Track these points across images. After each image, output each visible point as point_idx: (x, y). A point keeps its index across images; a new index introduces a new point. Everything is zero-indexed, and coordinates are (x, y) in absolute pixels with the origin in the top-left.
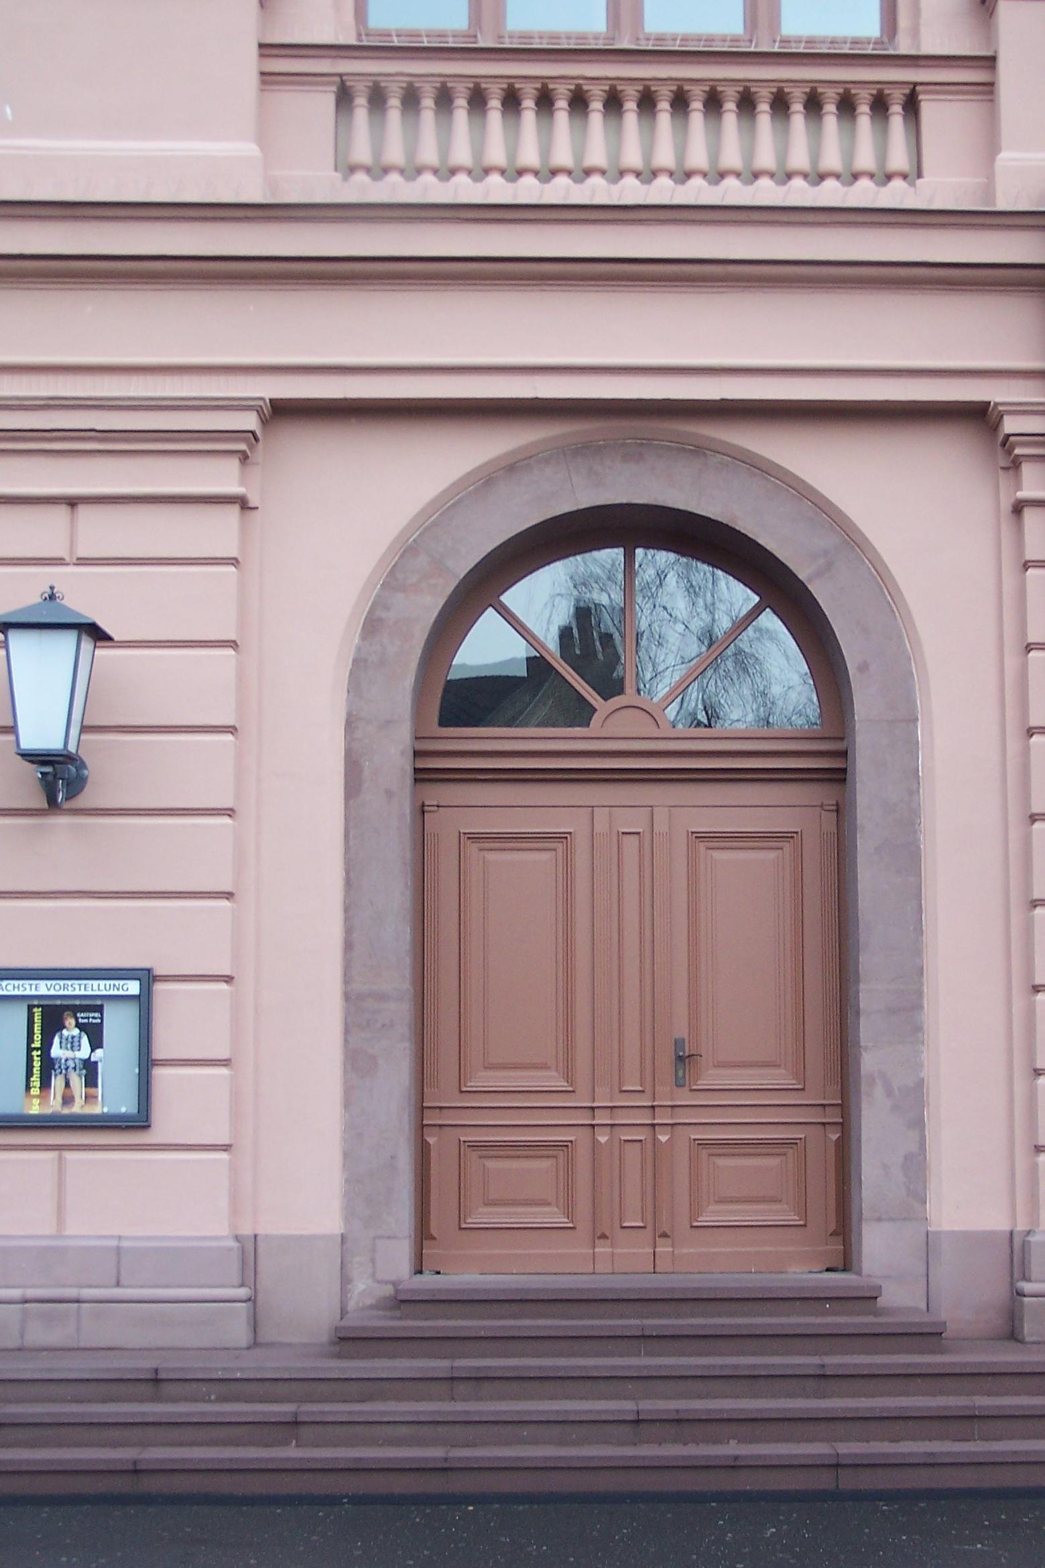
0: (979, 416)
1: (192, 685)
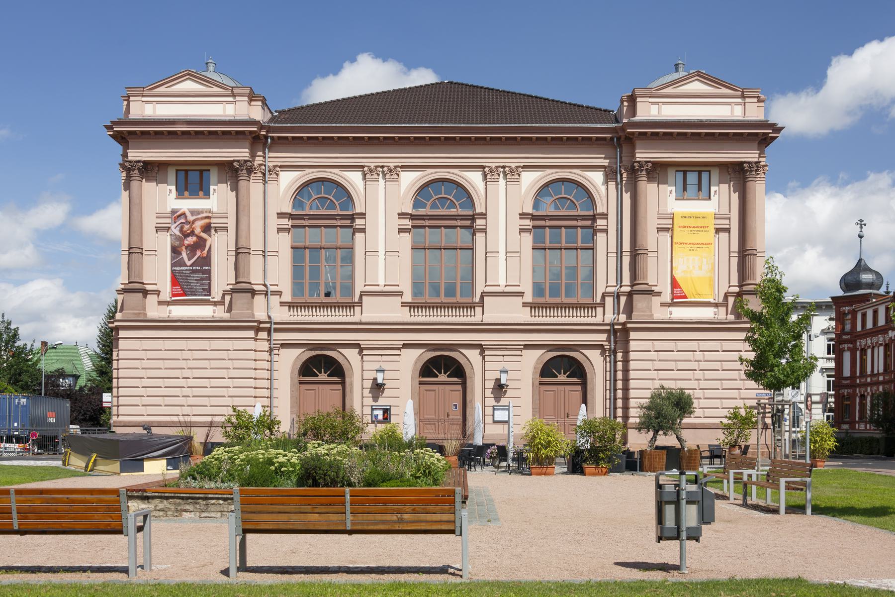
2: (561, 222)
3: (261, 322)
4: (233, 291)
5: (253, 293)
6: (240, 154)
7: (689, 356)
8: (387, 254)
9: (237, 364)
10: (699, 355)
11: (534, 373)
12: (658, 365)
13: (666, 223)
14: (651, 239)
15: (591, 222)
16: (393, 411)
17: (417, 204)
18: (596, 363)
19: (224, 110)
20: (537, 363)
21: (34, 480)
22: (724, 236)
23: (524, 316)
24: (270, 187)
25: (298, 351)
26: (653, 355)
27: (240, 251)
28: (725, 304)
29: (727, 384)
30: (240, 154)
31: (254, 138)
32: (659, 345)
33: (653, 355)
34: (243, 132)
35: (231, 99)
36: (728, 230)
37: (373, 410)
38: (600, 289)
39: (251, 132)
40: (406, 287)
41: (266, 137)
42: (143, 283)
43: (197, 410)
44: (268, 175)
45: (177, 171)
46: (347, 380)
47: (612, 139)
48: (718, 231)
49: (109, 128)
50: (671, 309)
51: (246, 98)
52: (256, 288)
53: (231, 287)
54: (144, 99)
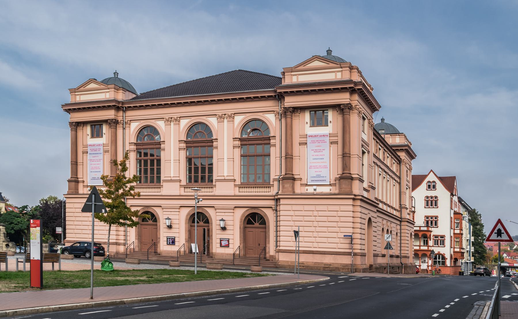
0: (271, 207)
1: (231, 223)
2: (254, 141)
3: (355, 195)
4: (284, 179)
5: (352, 179)
6: (110, 114)
7: (310, 213)
9: (343, 219)
10: (315, 213)
11: (241, 222)
12: (295, 218)
13: (303, 140)
14: (297, 150)
15: (266, 140)
16: (176, 240)
17: (188, 135)
18: (269, 214)
19: (106, 96)
20: (242, 217)
21: (304, 286)
22: (334, 146)
23: (237, 192)
24: (127, 130)
25: (189, 209)
26: (292, 213)
27: (345, 155)
28: (334, 185)
29: (330, 229)
30: (110, 114)
31: (352, 91)
32: (295, 208)
33: (292, 213)
34: (346, 88)
35: (340, 69)
36: (337, 143)
37: (221, 241)
38: (273, 176)
39: (350, 88)
40: (237, 177)
41: (123, 107)
43: (321, 245)
44: (126, 124)
45: (310, 111)
46: (158, 224)
47: (275, 96)
48: (331, 143)
49: (63, 106)
50: (307, 187)
51: (348, 69)
52: (353, 176)
54: (293, 73)
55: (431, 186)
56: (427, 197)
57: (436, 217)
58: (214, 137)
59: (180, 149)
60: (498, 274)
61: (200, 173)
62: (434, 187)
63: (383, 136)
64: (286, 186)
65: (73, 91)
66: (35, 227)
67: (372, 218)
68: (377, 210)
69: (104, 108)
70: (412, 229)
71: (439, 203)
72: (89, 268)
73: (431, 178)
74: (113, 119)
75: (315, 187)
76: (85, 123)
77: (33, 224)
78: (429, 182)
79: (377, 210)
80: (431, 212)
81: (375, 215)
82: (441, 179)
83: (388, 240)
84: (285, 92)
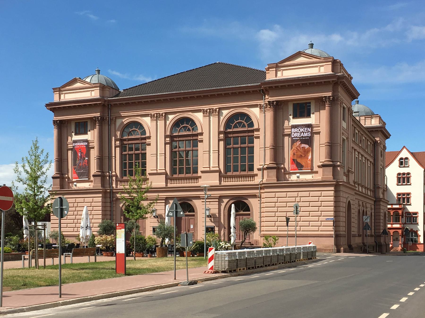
8: (321, 146)
24: (113, 126)
38: (256, 166)
42: (103, 172)
47: (260, 90)
53: (322, 163)
55: (403, 163)
56: (399, 174)
57: (409, 194)
58: (199, 131)
59: (219, 140)
60: (313, 136)
61: (182, 164)
62: (406, 163)
63: (358, 118)
64: (270, 174)
65: (59, 90)
66: (120, 229)
67: (351, 201)
68: (355, 193)
69: (319, 84)
70: (385, 208)
71: (412, 180)
72: (88, 261)
73: (404, 154)
74: (98, 117)
75: (298, 175)
76: (286, 102)
77: (119, 226)
78: (401, 159)
79: (355, 193)
80: (404, 189)
81: (354, 198)
82: (412, 154)
83: (366, 221)
84: (269, 87)
